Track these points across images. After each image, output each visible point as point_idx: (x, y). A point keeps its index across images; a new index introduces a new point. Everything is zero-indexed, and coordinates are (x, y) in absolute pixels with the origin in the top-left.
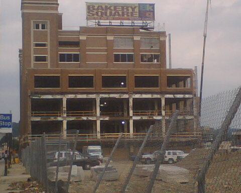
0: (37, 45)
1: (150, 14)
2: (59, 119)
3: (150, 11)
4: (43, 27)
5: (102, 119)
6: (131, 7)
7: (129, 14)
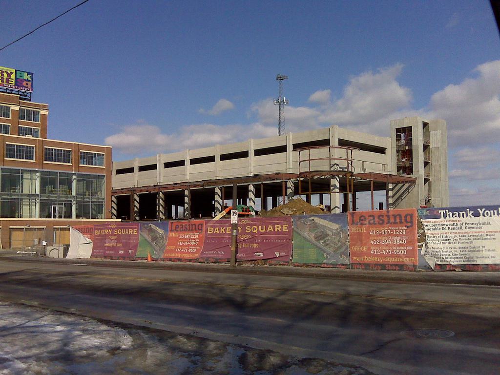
1: (27, 84)
6: (7, 73)
7: (5, 80)
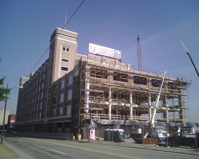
0: (63, 60)
1: (119, 56)
2: (107, 103)
3: (120, 54)
4: (68, 50)
5: (133, 106)
